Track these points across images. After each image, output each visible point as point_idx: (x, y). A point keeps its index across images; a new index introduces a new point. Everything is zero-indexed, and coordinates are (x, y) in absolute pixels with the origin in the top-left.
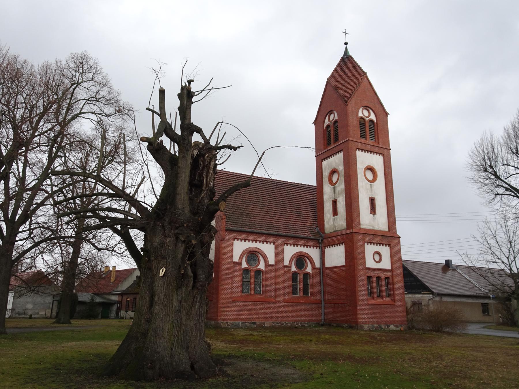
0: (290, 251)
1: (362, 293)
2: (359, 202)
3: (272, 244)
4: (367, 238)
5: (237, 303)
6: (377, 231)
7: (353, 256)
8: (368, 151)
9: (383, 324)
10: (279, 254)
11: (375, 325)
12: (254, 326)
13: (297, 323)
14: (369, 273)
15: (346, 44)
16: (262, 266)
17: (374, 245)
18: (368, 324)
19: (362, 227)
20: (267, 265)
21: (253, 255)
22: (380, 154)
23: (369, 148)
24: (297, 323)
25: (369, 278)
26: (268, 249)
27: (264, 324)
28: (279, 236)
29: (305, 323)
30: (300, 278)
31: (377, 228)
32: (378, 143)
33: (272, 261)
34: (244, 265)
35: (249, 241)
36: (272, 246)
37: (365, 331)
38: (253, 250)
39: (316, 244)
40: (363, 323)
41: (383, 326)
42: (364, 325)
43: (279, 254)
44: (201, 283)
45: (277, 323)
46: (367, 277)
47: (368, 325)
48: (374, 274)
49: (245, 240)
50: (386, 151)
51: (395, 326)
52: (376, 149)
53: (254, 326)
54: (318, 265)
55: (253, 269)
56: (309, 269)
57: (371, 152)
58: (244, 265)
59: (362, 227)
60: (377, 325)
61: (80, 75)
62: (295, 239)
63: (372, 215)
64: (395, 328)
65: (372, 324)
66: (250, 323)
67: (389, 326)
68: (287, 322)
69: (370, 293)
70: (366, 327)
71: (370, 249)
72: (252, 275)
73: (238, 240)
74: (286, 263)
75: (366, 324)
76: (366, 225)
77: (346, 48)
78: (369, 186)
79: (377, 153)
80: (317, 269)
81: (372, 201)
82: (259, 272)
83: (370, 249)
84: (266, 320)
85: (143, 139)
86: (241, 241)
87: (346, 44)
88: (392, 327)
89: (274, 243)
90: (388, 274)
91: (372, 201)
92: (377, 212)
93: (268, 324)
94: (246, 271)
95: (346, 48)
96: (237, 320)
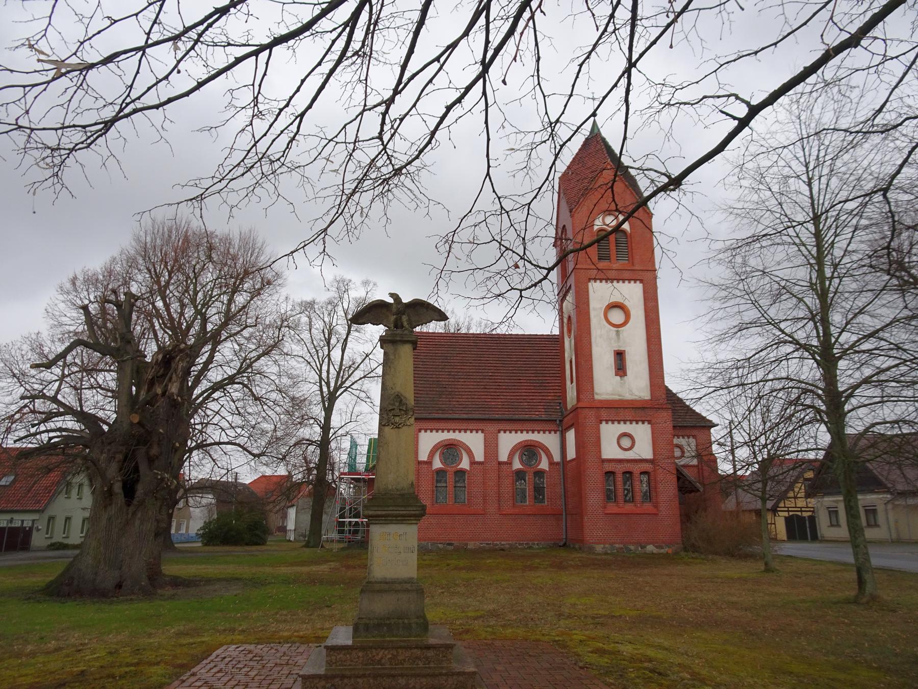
0: (508, 441)
1: (594, 498)
2: (591, 360)
3: (480, 432)
4: (604, 414)
6: (627, 401)
7: (589, 443)
9: (633, 544)
10: (491, 447)
11: (617, 546)
14: (608, 467)
16: (465, 464)
17: (619, 423)
18: (604, 543)
19: (596, 397)
20: (473, 463)
21: (450, 450)
22: (635, 281)
24: (520, 544)
25: (610, 474)
26: (474, 441)
27: (467, 544)
28: (489, 420)
30: (450, 478)
31: (628, 396)
32: (633, 264)
33: (479, 456)
35: (443, 431)
36: (480, 435)
37: (599, 554)
38: (450, 442)
39: (553, 427)
41: (632, 547)
42: (596, 546)
43: (491, 447)
46: (606, 473)
48: (619, 469)
49: (437, 431)
50: (649, 274)
52: (626, 275)
54: (557, 458)
55: (451, 470)
56: (544, 465)
58: (437, 464)
59: (597, 397)
60: (621, 546)
62: (515, 422)
63: (618, 378)
64: (655, 551)
65: (611, 544)
69: (610, 496)
70: (599, 548)
71: (609, 432)
72: (450, 478)
74: (503, 456)
76: (608, 394)
78: (614, 333)
79: (629, 281)
80: (558, 464)
81: (620, 356)
82: (462, 472)
83: (609, 432)
88: (650, 548)
89: (483, 431)
91: (620, 356)
92: (629, 372)
93: (471, 545)
94: (520, 475)
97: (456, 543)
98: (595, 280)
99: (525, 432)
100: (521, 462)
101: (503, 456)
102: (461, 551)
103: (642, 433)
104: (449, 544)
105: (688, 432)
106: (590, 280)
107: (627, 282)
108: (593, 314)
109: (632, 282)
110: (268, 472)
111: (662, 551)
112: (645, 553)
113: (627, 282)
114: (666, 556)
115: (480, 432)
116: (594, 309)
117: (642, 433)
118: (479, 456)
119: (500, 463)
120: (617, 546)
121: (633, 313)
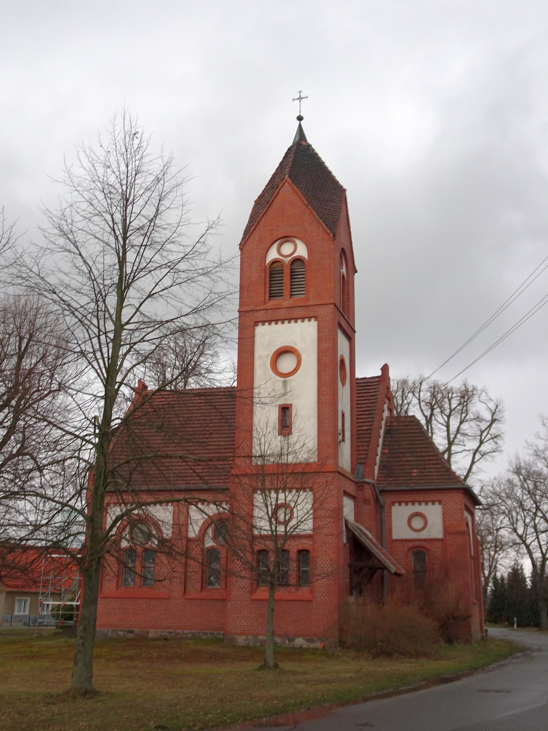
9: (280, 636)
15: (300, 118)
22: (310, 319)
23: (283, 313)
24: (203, 634)
26: (163, 514)
27: (148, 633)
34: (209, 543)
44: (176, 575)
45: (169, 632)
47: (244, 637)
51: (307, 640)
52: (298, 312)
61: (95, 282)
64: (305, 645)
66: (124, 631)
67: (291, 640)
68: (185, 632)
74: (193, 532)
75: (241, 634)
77: (300, 126)
78: (281, 384)
79: (303, 319)
87: (300, 118)
88: (299, 641)
89: (440, 502)
90: (306, 544)
95: (300, 126)
97: (137, 631)
99: (417, 504)
100: (215, 538)
101: (193, 532)
104: (130, 632)
105: (432, 496)
106: (256, 323)
109: (306, 320)
110: (528, 580)
113: (299, 321)
114: (314, 651)
115: (437, 503)
116: (260, 357)
117: (303, 504)
118: (167, 532)
121: (304, 358)
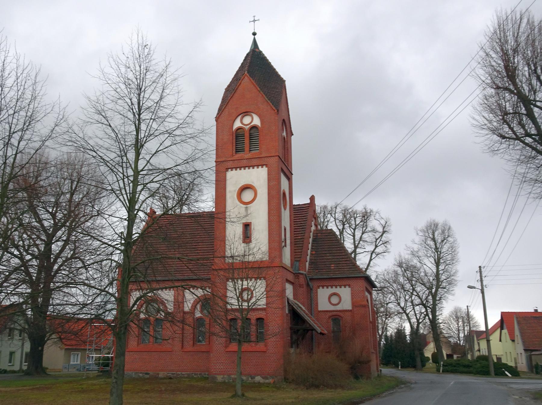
5: (131, 353)
8: (245, 167)
10: (179, 302)
11: (233, 376)
12: (147, 376)
13: (195, 374)
15: (254, 34)
18: (223, 375)
22: (262, 166)
24: (195, 374)
26: (168, 295)
27: (158, 374)
29: (205, 374)
33: (170, 307)
34: (198, 314)
40: (215, 374)
42: (217, 376)
45: (173, 374)
47: (222, 376)
51: (263, 378)
52: (254, 162)
53: (147, 376)
57: (249, 167)
64: (262, 381)
65: (229, 375)
68: (183, 373)
70: (220, 378)
73: (323, 287)
75: (219, 374)
77: (255, 39)
78: (244, 209)
79: (258, 166)
81: (247, 226)
84: (160, 371)
85: (312, 198)
86: (327, 288)
87: (254, 34)
88: (258, 379)
89: (349, 286)
90: (262, 315)
91: (247, 226)
93: (161, 375)
95: (255, 39)
96: (131, 371)
97: (151, 373)
98: (232, 169)
100: (201, 312)
101: (187, 307)
102: (155, 379)
103: (259, 288)
104: (146, 374)
106: (227, 169)
107: (256, 168)
108: (228, 195)
109: (260, 167)
111: (267, 381)
112: (254, 383)
113: (256, 168)
115: (347, 287)
116: (230, 192)
117: (259, 288)
119: (185, 313)
120: (233, 376)
